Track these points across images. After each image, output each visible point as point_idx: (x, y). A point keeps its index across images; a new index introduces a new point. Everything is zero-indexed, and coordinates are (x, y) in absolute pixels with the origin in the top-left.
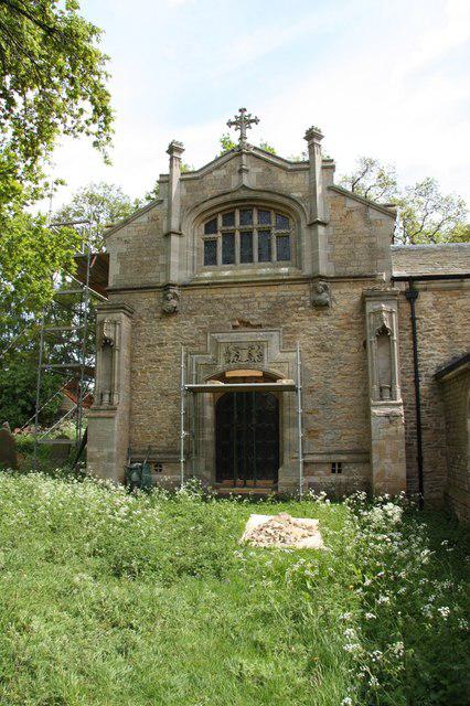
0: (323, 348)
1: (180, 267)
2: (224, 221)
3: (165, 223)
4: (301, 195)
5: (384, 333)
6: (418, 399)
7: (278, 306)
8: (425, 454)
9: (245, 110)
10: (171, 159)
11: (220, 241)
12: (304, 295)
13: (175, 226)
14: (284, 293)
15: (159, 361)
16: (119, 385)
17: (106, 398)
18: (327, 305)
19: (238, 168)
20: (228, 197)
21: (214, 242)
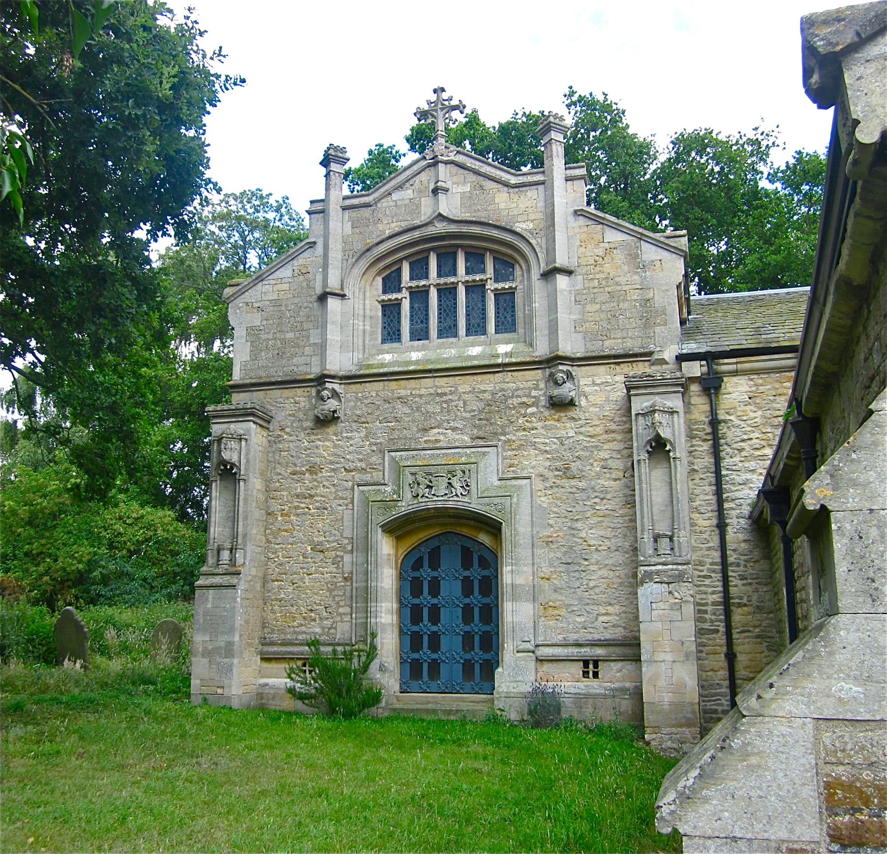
0: (566, 472)
1: (343, 347)
2: (439, 267)
3: (319, 278)
4: (531, 226)
5: (659, 447)
6: (724, 556)
7: (495, 404)
8: (737, 649)
9: (443, 90)
10: (327, 176)
11: (406, 305)
12: (536, 388)
13: (333, 283)
14: (505, 386)
15: (311, 496)
16: (245, 536)
17: (225, 555)
18: (571, 403)
19: (432, 186)
20: (416, 234)
21: (398, 304)
